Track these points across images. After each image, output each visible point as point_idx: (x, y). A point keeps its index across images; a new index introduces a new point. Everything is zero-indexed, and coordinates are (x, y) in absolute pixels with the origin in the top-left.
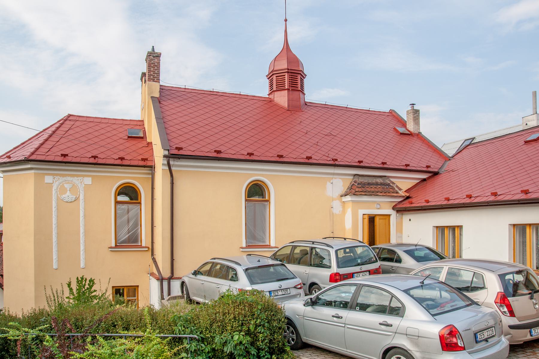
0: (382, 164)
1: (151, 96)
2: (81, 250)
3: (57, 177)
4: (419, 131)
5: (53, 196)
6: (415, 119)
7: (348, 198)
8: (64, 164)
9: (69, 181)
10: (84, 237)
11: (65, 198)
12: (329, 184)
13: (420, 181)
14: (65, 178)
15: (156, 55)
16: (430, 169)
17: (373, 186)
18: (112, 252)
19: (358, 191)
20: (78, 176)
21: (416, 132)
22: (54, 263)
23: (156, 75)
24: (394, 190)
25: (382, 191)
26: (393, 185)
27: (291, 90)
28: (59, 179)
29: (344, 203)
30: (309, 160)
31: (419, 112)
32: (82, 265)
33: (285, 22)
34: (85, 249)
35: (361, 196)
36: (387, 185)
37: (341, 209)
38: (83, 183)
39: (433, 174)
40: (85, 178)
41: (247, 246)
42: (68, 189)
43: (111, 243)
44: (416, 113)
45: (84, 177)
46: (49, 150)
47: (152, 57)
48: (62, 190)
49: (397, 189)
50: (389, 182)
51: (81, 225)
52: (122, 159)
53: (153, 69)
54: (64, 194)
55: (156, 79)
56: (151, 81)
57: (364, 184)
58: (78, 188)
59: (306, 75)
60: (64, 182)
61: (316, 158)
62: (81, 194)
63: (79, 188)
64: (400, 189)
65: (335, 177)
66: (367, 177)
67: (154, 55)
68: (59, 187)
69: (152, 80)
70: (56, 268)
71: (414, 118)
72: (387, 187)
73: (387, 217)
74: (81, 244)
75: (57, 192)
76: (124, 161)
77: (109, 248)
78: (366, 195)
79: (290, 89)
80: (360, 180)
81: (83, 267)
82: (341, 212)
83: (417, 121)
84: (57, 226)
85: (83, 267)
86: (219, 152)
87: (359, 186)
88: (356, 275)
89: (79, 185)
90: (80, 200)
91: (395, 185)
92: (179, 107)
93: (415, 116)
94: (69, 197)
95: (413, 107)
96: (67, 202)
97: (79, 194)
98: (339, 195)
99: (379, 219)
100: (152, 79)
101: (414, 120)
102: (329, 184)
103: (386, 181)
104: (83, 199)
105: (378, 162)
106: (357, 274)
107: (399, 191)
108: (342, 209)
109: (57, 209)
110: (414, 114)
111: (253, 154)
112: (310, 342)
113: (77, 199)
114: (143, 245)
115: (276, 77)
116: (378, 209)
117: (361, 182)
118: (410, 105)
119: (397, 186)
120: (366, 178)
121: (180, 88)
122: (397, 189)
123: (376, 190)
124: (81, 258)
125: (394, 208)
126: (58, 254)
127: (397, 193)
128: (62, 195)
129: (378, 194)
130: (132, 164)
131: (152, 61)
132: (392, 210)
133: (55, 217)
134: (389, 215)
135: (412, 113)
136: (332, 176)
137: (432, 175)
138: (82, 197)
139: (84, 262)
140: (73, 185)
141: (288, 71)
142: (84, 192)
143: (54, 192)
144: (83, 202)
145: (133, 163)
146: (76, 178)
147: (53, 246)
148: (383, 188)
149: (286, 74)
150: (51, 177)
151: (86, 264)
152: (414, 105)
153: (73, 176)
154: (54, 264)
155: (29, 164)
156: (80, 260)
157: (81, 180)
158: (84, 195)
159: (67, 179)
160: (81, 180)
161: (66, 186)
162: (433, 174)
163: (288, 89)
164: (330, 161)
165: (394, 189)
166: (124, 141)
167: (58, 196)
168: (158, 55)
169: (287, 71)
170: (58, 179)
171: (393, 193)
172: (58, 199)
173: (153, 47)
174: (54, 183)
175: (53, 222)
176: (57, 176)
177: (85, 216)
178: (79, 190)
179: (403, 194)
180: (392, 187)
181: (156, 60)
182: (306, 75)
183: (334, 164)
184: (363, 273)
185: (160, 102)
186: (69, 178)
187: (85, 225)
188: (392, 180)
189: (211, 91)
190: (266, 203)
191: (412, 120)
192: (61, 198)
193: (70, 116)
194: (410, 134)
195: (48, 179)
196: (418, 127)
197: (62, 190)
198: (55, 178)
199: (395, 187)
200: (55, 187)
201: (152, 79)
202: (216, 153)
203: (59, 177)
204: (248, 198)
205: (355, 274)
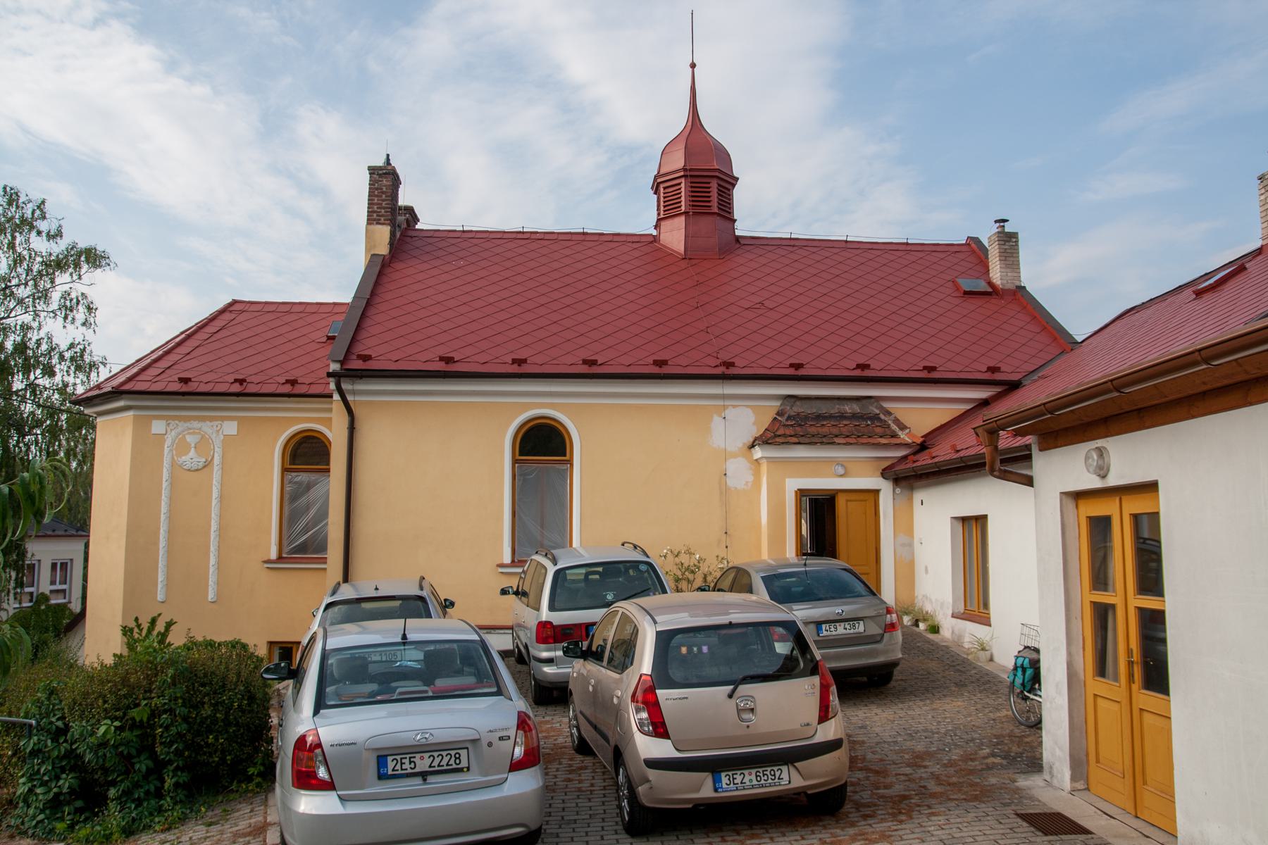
0: (654, 364)
1: (372, 253)
3: (173, 422)
4: (1017, 283)
5: (165, 459)
6: (1005, 254)
7: (758, 453)
8: (181, 397)
9: (194, 429)
10: (217, 539)
11: (185, 463)
12: (717, 420)
13: (975, 404)
14: (188, 424)
15: (384, 171)
16: (998, 376)
17: (828, 422)
18: (272, 573)
19: (784, 435)
20: (212, 419)
21: (1010, 286)
22: (159, 589)
23: (383, 211)
24: (887, 430)
25: (850, 432)
26: (886, 419)
27: (691, 213)
29: (759, 463)
30: (522, 367)
31: (1017, 238)
32: (211, 596)
33: (691, 69)
34: (219, 563)
35: (784, 446)
36: (870, 418)
37: (751, 478)
38: (221, 432)
39: (1007, 387)
41: (516, 561)
42: (193, 445)
44: (1008, 240)
45: (223, 421)
46: (163, 371)
47: (377, 177)
48: (182, 448)
49: (894, 427)
50: (878, 412)
51: (213, 515)
52: (293, 382)
53: (378, 200)
54: (183, 455)
55: (382, 219)
56: (373, 224)
57: (806, 418)
59: (737, 179)
60: (186, 432)
61: (471, 361)
62: (216, 453)
64: (903, 427)
65: (727, 403)
66: (818, 402)
67: (380, 172)
69: (375, 222)
70: (161, 600)
71: (1002, 254)
72: (869, 422)
73: (871, 496)
75: (171, 450)
76: (297, 386)
78: (799, 443)
79: (689, 212)
80: (795, 409)
81: (212, 601)
82: (750, 484)
83: (1012, 259)
84: (169, 517)
85: (212, 599)
86: (448, 360)
87: (789, 423)
88: (828, 628)
89: (213, 437)
91: (892, 417)
92: (536, 279)
93: (1006, 247)
95: (1003, 226)
96: (189, 470)
97: (212, 453)
98: (744, 444)
99: (847, 501)
100: (374, 220)
101: (1003, 258)
102: (717, 420)
103: (871, 408)
105: (847, 366)
106: (828, 625)
107: (900, 433)
108: (752, 477)
109: (171, 484)
110: (1003, 243)
111: (732, 364)
113: (208, 465)
115: (665, 188)
116: (841, 476)
117: (798, 414)
118: (996, 222)
119: (897, 421)
120: (814, 403)
121: (455, 231)
122: (894, 427)
123: (835, 431)
124: (210, 583)
125: (885, 473)
126: (168, 573)
127: (892, 437)
128: (181, 458)
129: (837, 440)
130: (263, 391)
131: (376, 184)
132: (882, 479)
133: (165, 499)
134: (877, 492)
135: (997, 243)
136: (720, 403)
137: (1005, 390)
138: (217, 460)
139: (216, 589)
140: (203, 437)
141: (686, 174)
142: (223, 450)
143: (166, 450)
144: (218, 470)
145: (266, 389)
146: (208, 423)
148: (856, 425)
149: (683, 180)
150: (235, 424)
151: (219, 594)
152: (1006, 223)
153: (203, 419)
154: (159, 592)
155: (122, 399)
158: (223, 457)
159: (190, 426)
161: (189, 439)
162: (1007, 387)
163: (686, 213)
164: (717, 369)
165: (889, 426)
166: (318, 346)
167: (173, 458)
169: (682, 174)
170: (175, 426)
171: (881, 437)
172: (173, 464)
173: (388, 155)
174: (168, 433)
175: (162, 509)
176: (173, 420)
177: (221, 498)
178: (212, 447)
179: (907, 439)
180: (881, 423)
181: (384, 182)
182: (737, 179)
183: (727, 373)
184: (847, 623)
186: (196, 424)
187: (221, 517)
188: (886, 405)
189: (520, 232)
190: (564, 467)
191: (998, 259)
193: (235, 302)
194: (994, 292)
195: (158, 427)
196: (1015, 274)
197: (182, 448)
198: (171, 425)
199: (890, 422)
200: (168, 442)
201: (374, 220)
202: (444, 362)
203: (177, 422)
204: (520, 455)
205: (824, 626)
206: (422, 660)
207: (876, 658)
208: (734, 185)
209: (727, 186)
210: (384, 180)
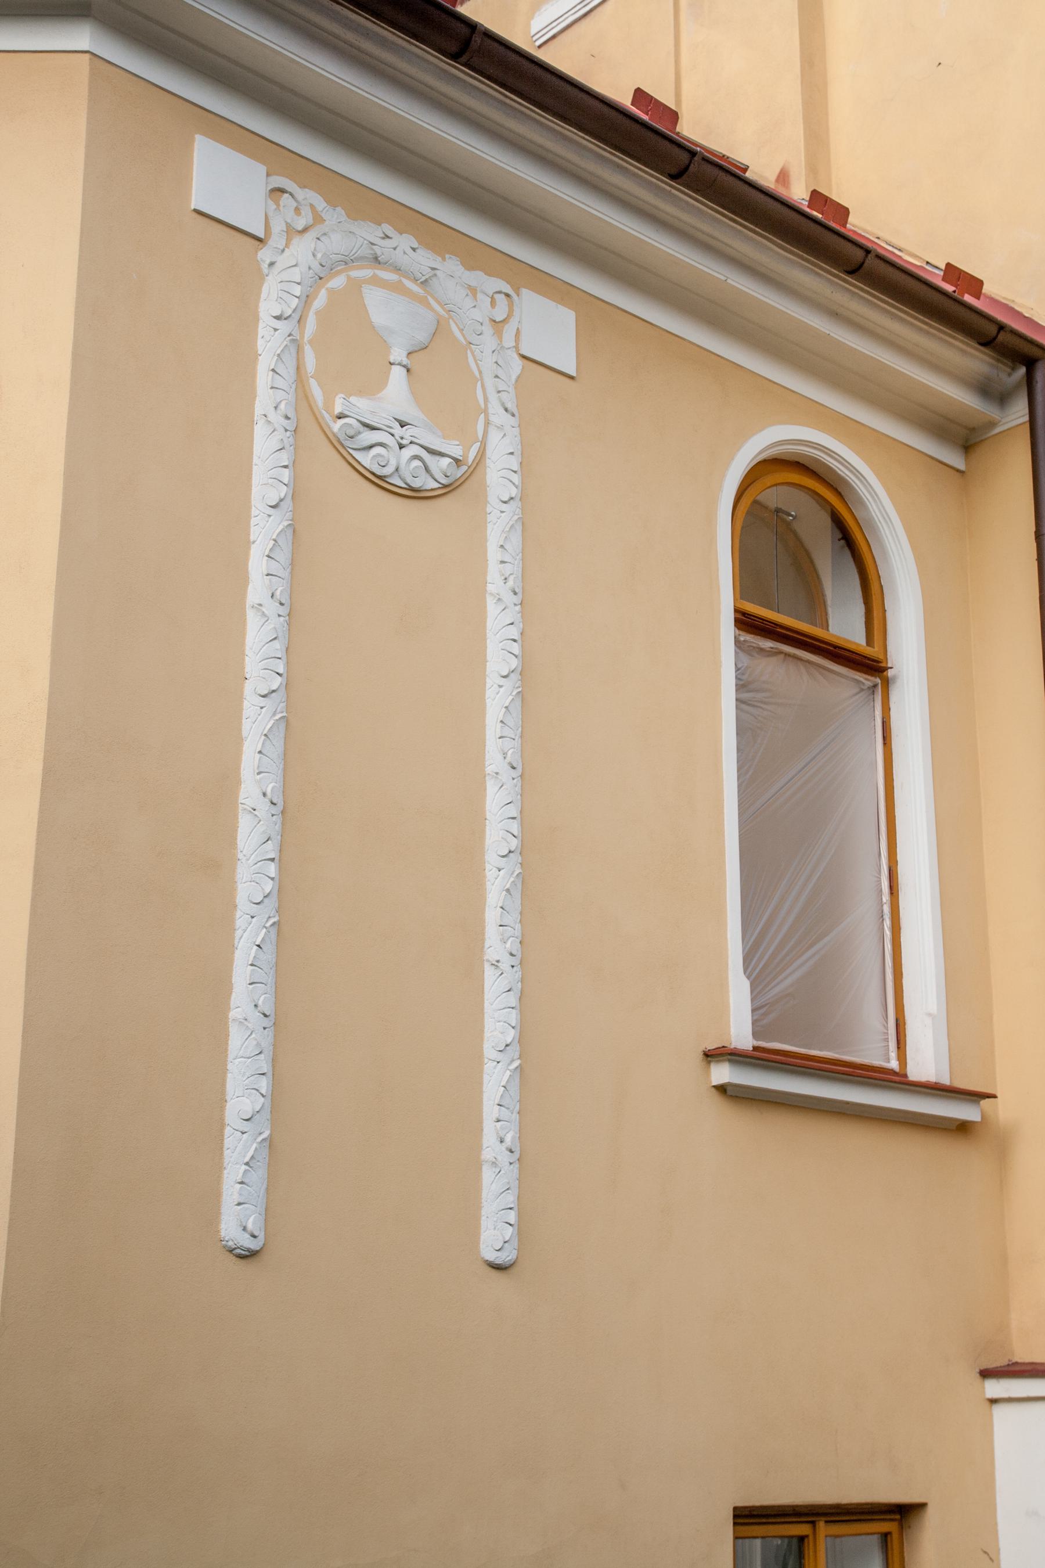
2: (489, 1052)
28: (318, 219)
40: (524, 291)
42: (398, 354)
58: (477, 374)
63: (480, 372)
68: (320, 301)
74: (489, 973)
75: (296, 344)
77: (711, 1056)
81: (502, 1258)
90: (486, 502)
94: (407, 433)
104: (514, 492)
147: (231, 948)
156: (478, 1166)
157: (493, 303)
159: (384, 248)
185: (493, 352)
192: (337, 426)
203: (320, 204)
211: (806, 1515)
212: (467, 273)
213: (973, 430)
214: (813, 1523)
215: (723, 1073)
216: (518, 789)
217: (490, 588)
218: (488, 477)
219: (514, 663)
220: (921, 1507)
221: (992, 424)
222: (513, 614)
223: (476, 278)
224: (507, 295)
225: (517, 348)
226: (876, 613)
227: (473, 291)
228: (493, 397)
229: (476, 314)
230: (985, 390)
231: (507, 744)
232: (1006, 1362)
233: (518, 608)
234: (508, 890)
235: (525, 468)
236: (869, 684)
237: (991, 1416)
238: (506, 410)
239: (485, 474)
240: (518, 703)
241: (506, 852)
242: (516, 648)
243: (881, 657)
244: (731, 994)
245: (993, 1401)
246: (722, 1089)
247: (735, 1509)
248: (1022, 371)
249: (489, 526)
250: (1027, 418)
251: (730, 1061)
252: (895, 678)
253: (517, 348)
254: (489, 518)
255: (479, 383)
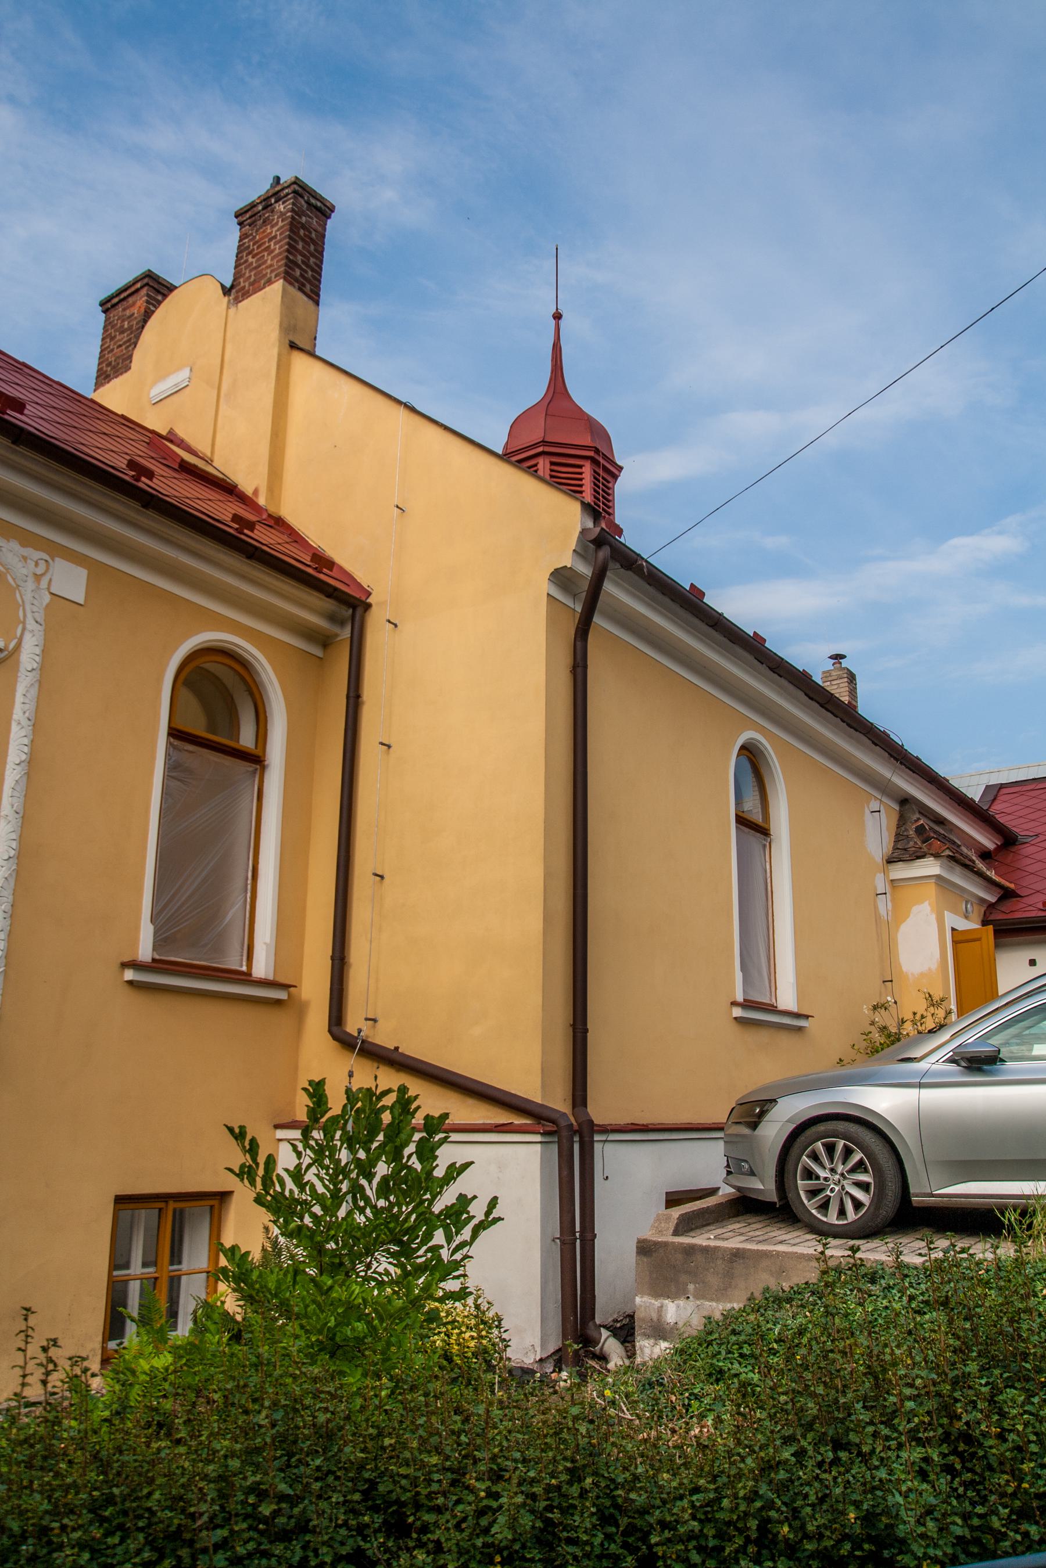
1: (292, 339)
15: (319, 204)
20: (27, 539)
33: (553, 322)
40: (57, 559)
43: (135, 942)
47: (305, 206)
59: (620, 469)
63: (23, 601)
67: (313, 201)
69: (296, 285)
77: (125, 965)
90: (18, 670)
97: (19, 634)
104: (35, 665)
112: (982, 1204)
114: (261, 968)
146: (14, 545)
157: (37, 564)
160: (37, 564)
168: (323, 208)
182: (620, 469)
206: (605, 1130)
207: (998, 1076)
208: (615, 477)
209: (609, 478)
210: (315, 219)
211: (164, 1198)
212: (22, 549)
213: (328, 637)
214: (167, 1202)
215: (129, 975)
216: (20, 824)
217: (15, 717)
218: (21, 657)
219: (24, 757)
220: (232, 1192)
221: (337, 635)
222: (28, 730)
223: (28, 551)
224: (46, 561)
225: (48, 589)
226: (261, 731)
227: (25, 558)
228: (29, 615)
229: (24, 571)
230: (332, 618)
231: (15, 800)
232: (290, 1120)
233: (30, 728)
234: (6, 878)
235: (45, 653)
236: (251, 769)
237: (278, 1147)
238: (37, 622)
239: (19, 656)
240: (25, 779)
241: (6, 858)
242: (26, 749)
243: (260, 754)
244: (142, 933)
245: (280, 1140)
246: (130, 983)
247: (116, 1196)
248: (351, 611)
249: (18, 684)
250: (349, 635)
251: (133, 968)
252: (268, 765)
253: (48, 589)
254: (19, 679)
255: (21, 608)
